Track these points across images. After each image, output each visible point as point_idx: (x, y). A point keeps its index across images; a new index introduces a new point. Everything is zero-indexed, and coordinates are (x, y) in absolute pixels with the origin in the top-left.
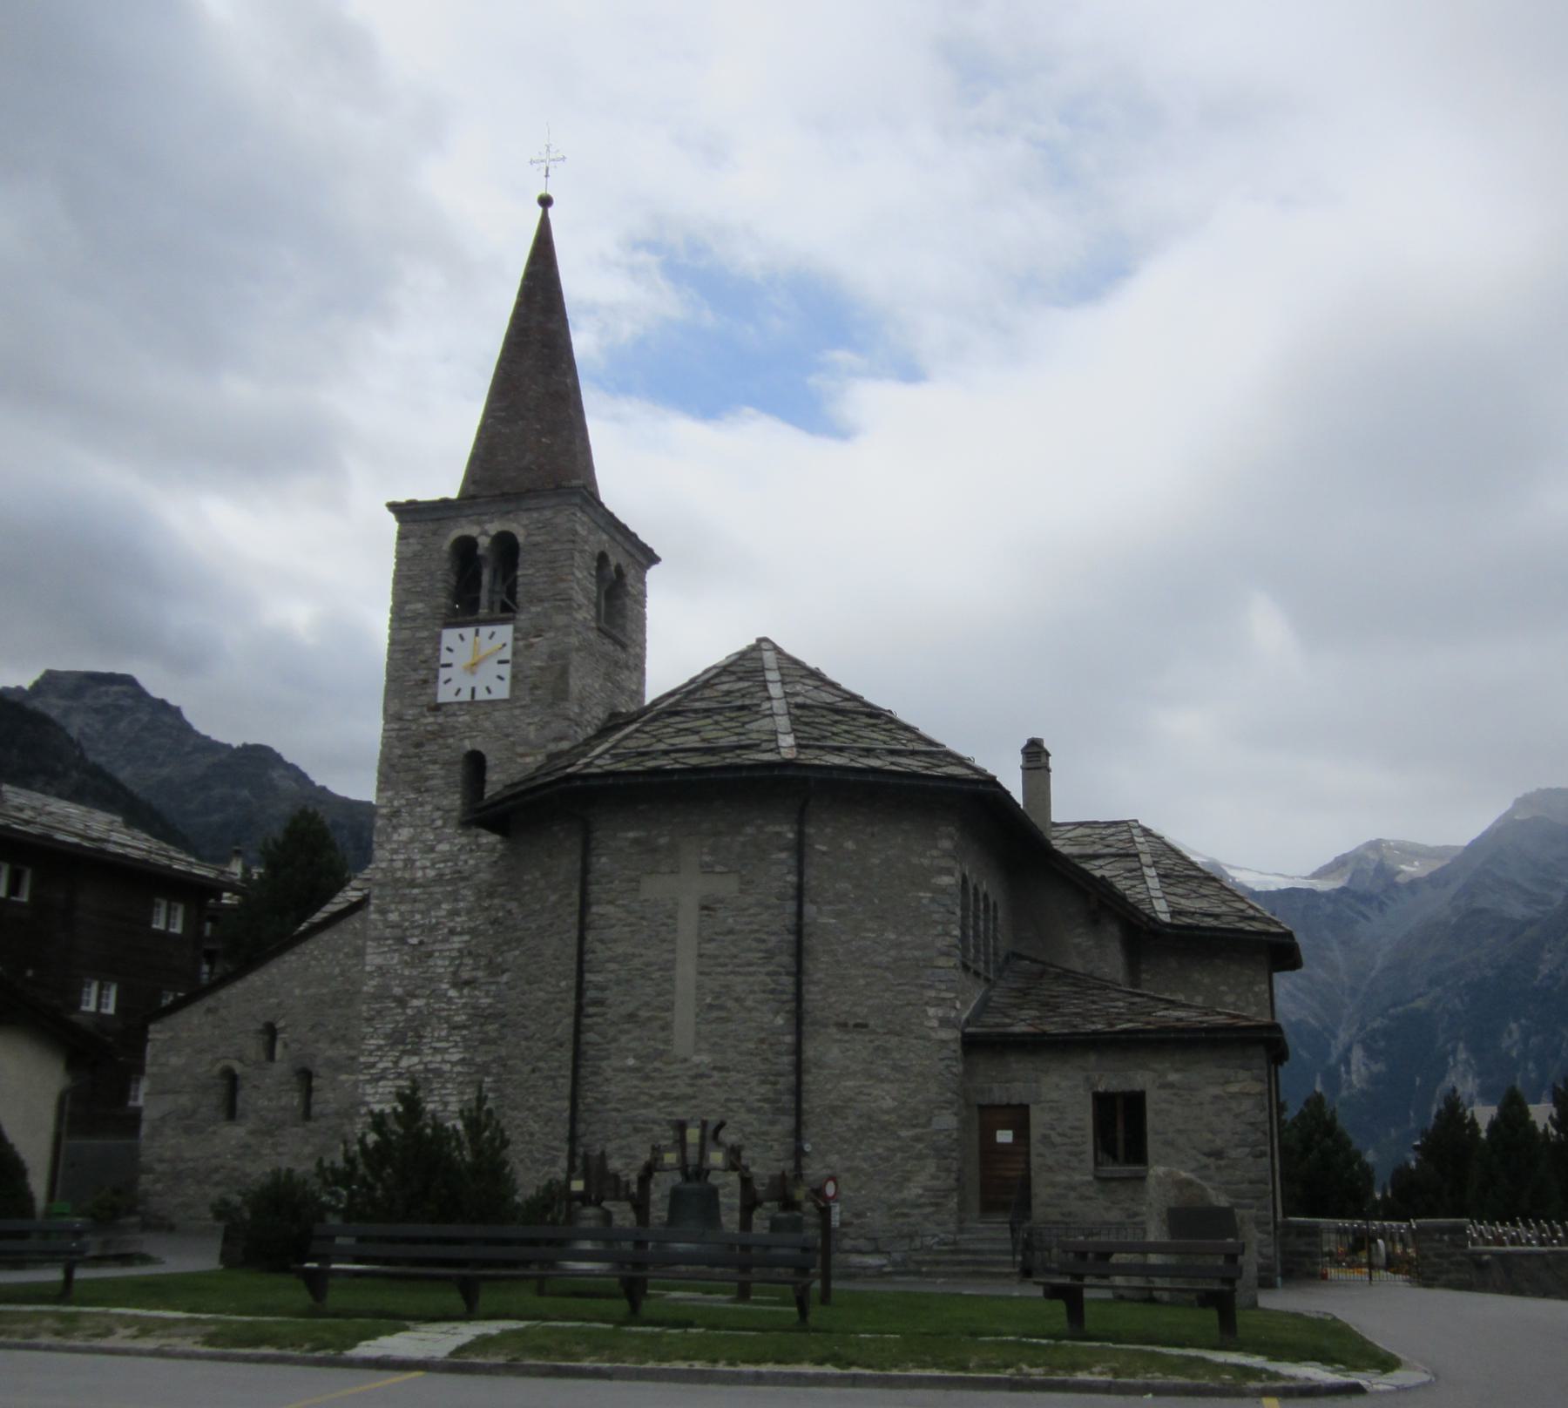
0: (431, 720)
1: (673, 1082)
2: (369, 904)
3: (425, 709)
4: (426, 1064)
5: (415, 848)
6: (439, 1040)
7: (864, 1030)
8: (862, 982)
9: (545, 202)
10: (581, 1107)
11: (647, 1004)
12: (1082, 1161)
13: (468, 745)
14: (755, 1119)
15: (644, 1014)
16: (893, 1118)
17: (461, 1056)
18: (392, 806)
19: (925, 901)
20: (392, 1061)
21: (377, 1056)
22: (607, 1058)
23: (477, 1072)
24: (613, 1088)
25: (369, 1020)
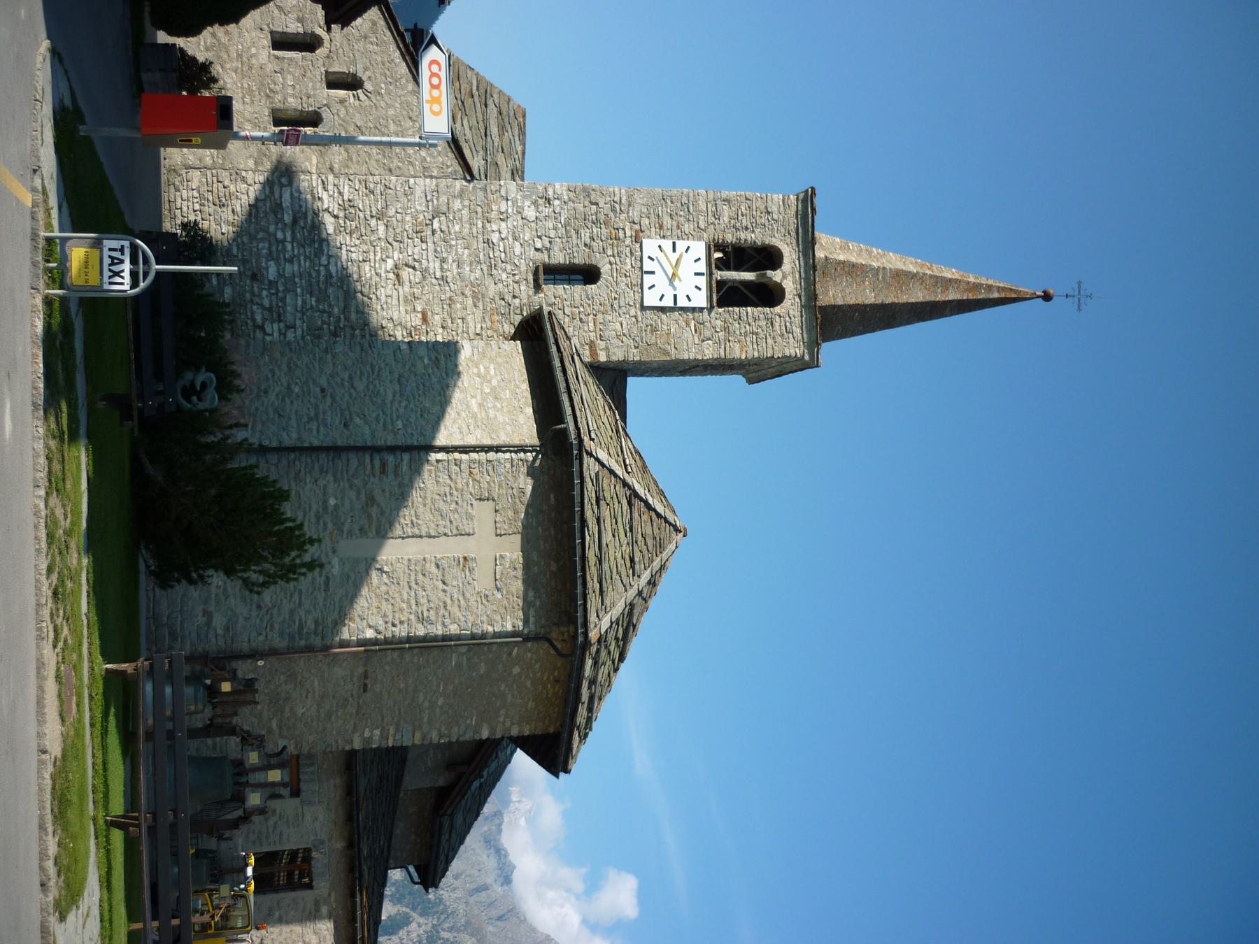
7: (362, 690)
8: (402, 686)
9: (1047, 297)
10: (292, 456)
11: (382, 513)
12: (254, 842)
13: (605, 269)
14: (285, 618)
15: (374, 511)
16: (287, 714)
17: (334, 274)
19: (468, 721)
20: (329, 207)
22: (335, 480)
23: (320, 289)
24: (309, 486)
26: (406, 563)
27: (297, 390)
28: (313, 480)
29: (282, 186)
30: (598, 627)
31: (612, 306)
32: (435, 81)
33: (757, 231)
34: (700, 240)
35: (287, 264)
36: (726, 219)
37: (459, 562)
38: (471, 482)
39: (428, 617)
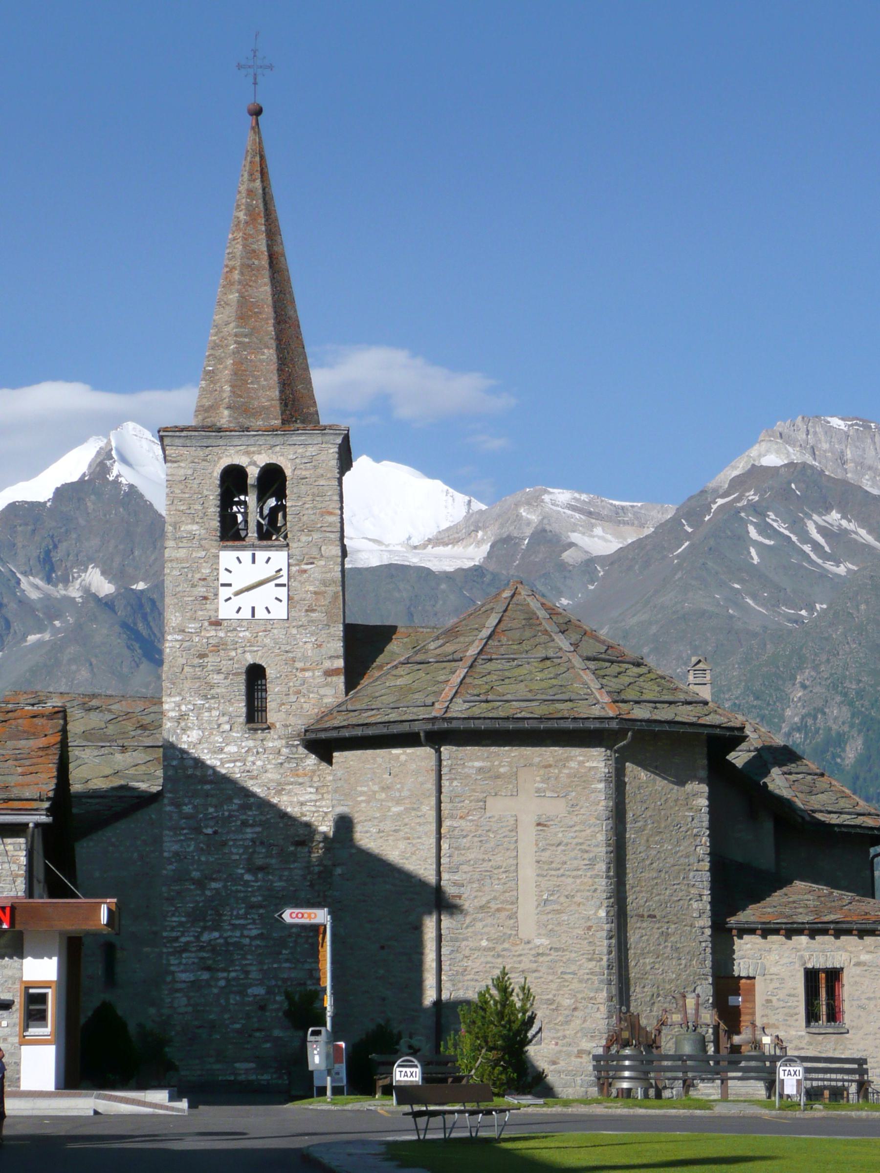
0: (213, 633)
1: (519, 959)
2: (164, 797)
3: (206, 624)
4: (226, 938)
5: (203, 748)
6: (238, 917)
9: (257, 112)
11: (495, 898)
13: (250, 659)
17: (259, 932)
18: (180, 710)
20: (194, 936)
21: (179, 931)
25: (170, 900)
26: (540, 879)
27: (381, 972)
28: (465, 960)
29: (174, 981)
30: (604, 705)
31: (287, 652)
32: (300, 915)
33: (206, 493)
34: (218, 556)
35: (250, 976)
36: (195, 527)
37: (541, 830)
38: (470, 817)
39: (590, 860)
